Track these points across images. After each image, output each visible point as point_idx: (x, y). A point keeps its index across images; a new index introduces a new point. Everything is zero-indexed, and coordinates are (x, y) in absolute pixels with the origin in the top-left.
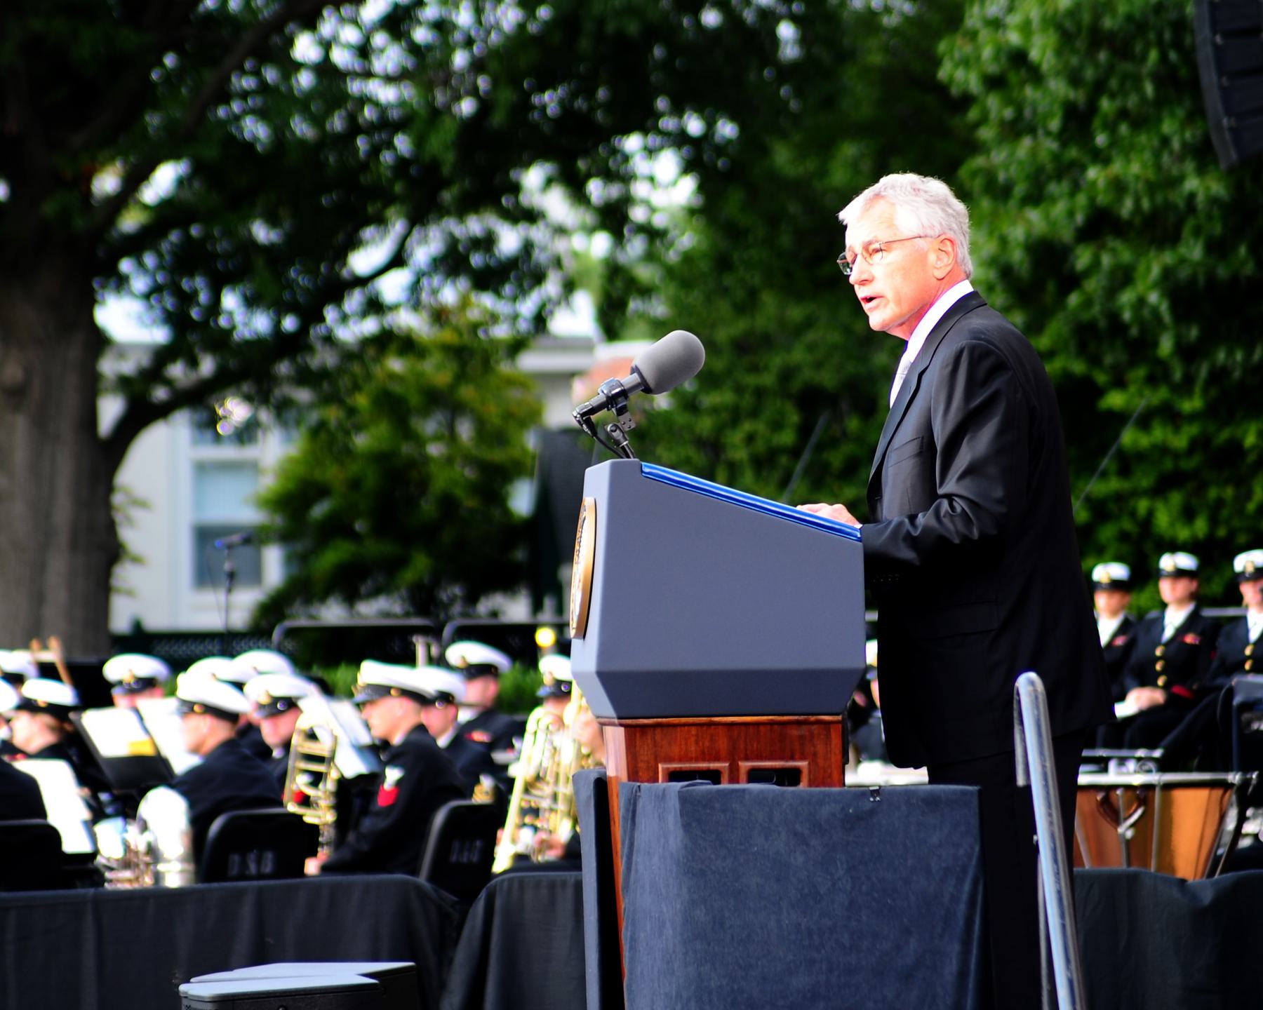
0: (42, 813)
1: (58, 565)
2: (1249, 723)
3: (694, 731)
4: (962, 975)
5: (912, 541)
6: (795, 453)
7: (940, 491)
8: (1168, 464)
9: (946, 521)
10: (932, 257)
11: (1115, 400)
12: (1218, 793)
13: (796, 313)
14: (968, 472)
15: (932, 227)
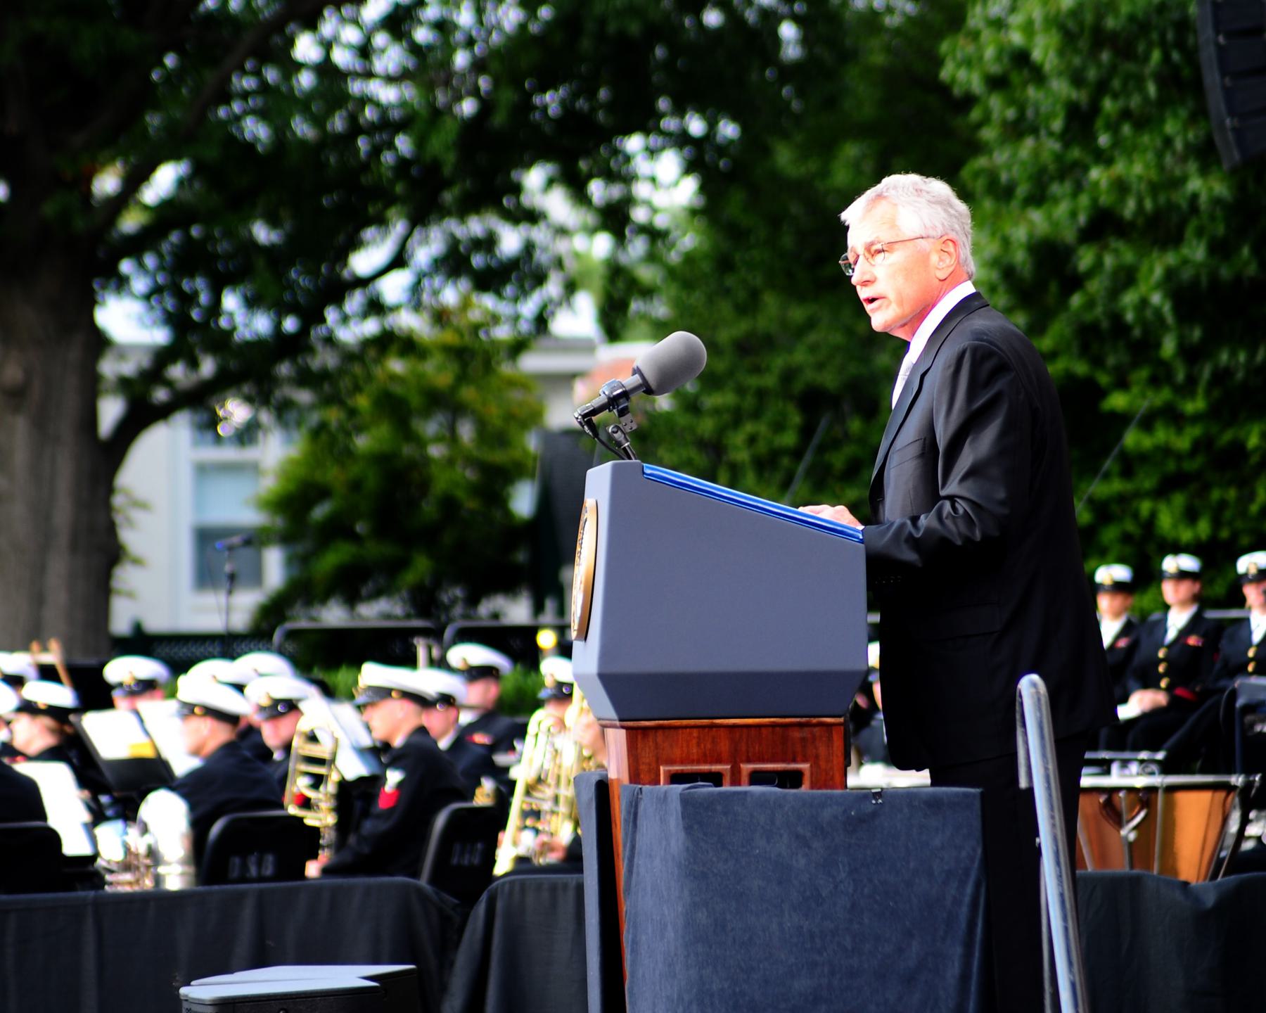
0: (42, 816)
1: (59, 567)
2: (1252, 725)
3: (695, 733)
4: (965, 977)
5: (914, 543)
6: (797, 454)
7: (943, 493)
8: (1171, 466)
9: (948, 522)
10: (934, 258)
11: (1118, 401)
12: (1221, 795)
13: (798, 314)
14: (971, 474)
15: (934, 228)
